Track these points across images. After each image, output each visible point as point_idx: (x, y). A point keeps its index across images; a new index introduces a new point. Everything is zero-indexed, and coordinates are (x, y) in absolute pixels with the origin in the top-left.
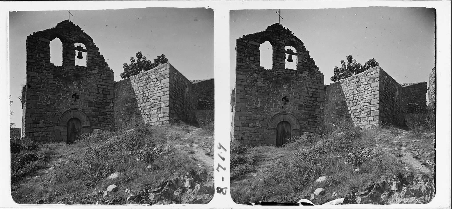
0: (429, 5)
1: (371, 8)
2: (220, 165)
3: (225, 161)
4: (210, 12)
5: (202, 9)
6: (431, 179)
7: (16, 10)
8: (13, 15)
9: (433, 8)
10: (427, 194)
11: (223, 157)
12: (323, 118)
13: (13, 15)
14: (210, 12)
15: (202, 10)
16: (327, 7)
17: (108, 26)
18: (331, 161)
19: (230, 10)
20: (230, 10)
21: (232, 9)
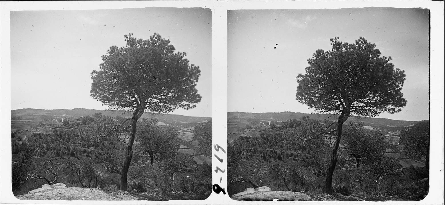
0: (423, 6)
1: (367, 9)
2: (218, 167)
3: (223, 162)
4: (208, 12)
5: (200, 9)
6: (423, 174)
7: (17, 10)
8: (14, 15)
9: (208, 9)
10: (421, 191)
11: (221, 159)
12: (172, 132)
13: (14, 15)
14: (208, 12)
15: (200, 9)
16: (323, 8)
17: (104, 25)
18: (168, 187)
19: (228, 10)
20: (228, 10)
21: (13, 11)
